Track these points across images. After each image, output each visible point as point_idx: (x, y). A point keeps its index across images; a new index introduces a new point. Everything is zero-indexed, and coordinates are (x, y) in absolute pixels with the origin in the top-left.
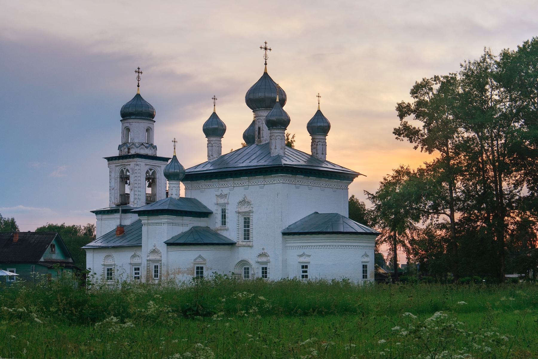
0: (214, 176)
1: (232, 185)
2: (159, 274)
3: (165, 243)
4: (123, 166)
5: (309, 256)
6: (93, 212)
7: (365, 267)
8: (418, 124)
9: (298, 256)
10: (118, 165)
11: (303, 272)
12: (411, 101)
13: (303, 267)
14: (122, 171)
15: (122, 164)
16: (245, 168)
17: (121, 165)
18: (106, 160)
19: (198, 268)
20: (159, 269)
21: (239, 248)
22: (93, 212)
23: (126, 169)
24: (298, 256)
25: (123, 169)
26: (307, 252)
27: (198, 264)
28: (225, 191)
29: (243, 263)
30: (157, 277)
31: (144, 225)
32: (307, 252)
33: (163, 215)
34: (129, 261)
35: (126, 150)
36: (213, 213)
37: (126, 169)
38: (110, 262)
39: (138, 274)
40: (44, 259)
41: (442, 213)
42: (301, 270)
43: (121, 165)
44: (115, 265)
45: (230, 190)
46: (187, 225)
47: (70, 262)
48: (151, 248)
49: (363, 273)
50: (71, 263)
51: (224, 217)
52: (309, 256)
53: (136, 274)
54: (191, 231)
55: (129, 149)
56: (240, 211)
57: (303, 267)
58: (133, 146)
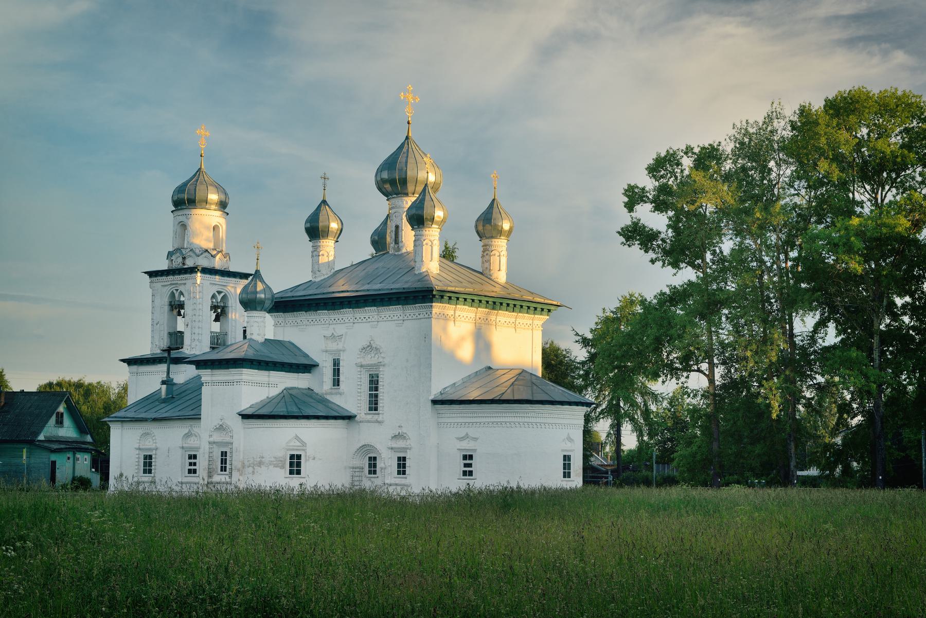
0: (232, 362)
1: (351, 320)
2: (228, 466)
3: (240, 415)
4: (174, 286)
5: (475, 439)
6: (124, 361)
7: (567, 458)
8: (658, 222)
9: (458, 439)
10: (166, 283)
11: (466, 465)
12: (649, 184)
13: (465, 457)
14: (173, 294)
15: (172, 282)
16: (391, 292)
17: (171, 284)
18: (147, 276)
19: (292, 457)
20: (228, 458)
21: (361, 424)
22: (124, 361)
23: (179, 291)
24: (458, 439)
25: (175, 291)
26: (472, 432)
27: (293, 450)
28: (340, 329)
29: (366, 449)
30: (225, 471)
31: (205, 384)
32: (472, 432)
33: (236, 368)
34: (180, 443)
35: (180, 260)
36: (318, 366)
37: (179, 291)
38: (148, 444)
39: (195, 464)
40: (45, 437)
41: (694, 371)
42: (188, 461)
43: (171, 284)
44: (156, 449)
45: (347, 329)
46: (232, 384)
47: (88, 441)
48: (217, 422)
49: (564, 468)
50: (89, 443)
51: (337, 372)
52: (475, 439)
53: (190, 464)
54: (282, 395)
55: (184, 258)
56: (364, 363)
57: (465, 457)
58: (191, 253)
